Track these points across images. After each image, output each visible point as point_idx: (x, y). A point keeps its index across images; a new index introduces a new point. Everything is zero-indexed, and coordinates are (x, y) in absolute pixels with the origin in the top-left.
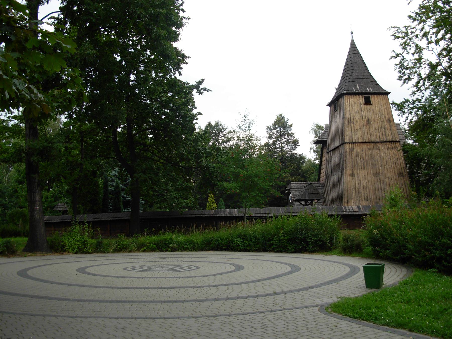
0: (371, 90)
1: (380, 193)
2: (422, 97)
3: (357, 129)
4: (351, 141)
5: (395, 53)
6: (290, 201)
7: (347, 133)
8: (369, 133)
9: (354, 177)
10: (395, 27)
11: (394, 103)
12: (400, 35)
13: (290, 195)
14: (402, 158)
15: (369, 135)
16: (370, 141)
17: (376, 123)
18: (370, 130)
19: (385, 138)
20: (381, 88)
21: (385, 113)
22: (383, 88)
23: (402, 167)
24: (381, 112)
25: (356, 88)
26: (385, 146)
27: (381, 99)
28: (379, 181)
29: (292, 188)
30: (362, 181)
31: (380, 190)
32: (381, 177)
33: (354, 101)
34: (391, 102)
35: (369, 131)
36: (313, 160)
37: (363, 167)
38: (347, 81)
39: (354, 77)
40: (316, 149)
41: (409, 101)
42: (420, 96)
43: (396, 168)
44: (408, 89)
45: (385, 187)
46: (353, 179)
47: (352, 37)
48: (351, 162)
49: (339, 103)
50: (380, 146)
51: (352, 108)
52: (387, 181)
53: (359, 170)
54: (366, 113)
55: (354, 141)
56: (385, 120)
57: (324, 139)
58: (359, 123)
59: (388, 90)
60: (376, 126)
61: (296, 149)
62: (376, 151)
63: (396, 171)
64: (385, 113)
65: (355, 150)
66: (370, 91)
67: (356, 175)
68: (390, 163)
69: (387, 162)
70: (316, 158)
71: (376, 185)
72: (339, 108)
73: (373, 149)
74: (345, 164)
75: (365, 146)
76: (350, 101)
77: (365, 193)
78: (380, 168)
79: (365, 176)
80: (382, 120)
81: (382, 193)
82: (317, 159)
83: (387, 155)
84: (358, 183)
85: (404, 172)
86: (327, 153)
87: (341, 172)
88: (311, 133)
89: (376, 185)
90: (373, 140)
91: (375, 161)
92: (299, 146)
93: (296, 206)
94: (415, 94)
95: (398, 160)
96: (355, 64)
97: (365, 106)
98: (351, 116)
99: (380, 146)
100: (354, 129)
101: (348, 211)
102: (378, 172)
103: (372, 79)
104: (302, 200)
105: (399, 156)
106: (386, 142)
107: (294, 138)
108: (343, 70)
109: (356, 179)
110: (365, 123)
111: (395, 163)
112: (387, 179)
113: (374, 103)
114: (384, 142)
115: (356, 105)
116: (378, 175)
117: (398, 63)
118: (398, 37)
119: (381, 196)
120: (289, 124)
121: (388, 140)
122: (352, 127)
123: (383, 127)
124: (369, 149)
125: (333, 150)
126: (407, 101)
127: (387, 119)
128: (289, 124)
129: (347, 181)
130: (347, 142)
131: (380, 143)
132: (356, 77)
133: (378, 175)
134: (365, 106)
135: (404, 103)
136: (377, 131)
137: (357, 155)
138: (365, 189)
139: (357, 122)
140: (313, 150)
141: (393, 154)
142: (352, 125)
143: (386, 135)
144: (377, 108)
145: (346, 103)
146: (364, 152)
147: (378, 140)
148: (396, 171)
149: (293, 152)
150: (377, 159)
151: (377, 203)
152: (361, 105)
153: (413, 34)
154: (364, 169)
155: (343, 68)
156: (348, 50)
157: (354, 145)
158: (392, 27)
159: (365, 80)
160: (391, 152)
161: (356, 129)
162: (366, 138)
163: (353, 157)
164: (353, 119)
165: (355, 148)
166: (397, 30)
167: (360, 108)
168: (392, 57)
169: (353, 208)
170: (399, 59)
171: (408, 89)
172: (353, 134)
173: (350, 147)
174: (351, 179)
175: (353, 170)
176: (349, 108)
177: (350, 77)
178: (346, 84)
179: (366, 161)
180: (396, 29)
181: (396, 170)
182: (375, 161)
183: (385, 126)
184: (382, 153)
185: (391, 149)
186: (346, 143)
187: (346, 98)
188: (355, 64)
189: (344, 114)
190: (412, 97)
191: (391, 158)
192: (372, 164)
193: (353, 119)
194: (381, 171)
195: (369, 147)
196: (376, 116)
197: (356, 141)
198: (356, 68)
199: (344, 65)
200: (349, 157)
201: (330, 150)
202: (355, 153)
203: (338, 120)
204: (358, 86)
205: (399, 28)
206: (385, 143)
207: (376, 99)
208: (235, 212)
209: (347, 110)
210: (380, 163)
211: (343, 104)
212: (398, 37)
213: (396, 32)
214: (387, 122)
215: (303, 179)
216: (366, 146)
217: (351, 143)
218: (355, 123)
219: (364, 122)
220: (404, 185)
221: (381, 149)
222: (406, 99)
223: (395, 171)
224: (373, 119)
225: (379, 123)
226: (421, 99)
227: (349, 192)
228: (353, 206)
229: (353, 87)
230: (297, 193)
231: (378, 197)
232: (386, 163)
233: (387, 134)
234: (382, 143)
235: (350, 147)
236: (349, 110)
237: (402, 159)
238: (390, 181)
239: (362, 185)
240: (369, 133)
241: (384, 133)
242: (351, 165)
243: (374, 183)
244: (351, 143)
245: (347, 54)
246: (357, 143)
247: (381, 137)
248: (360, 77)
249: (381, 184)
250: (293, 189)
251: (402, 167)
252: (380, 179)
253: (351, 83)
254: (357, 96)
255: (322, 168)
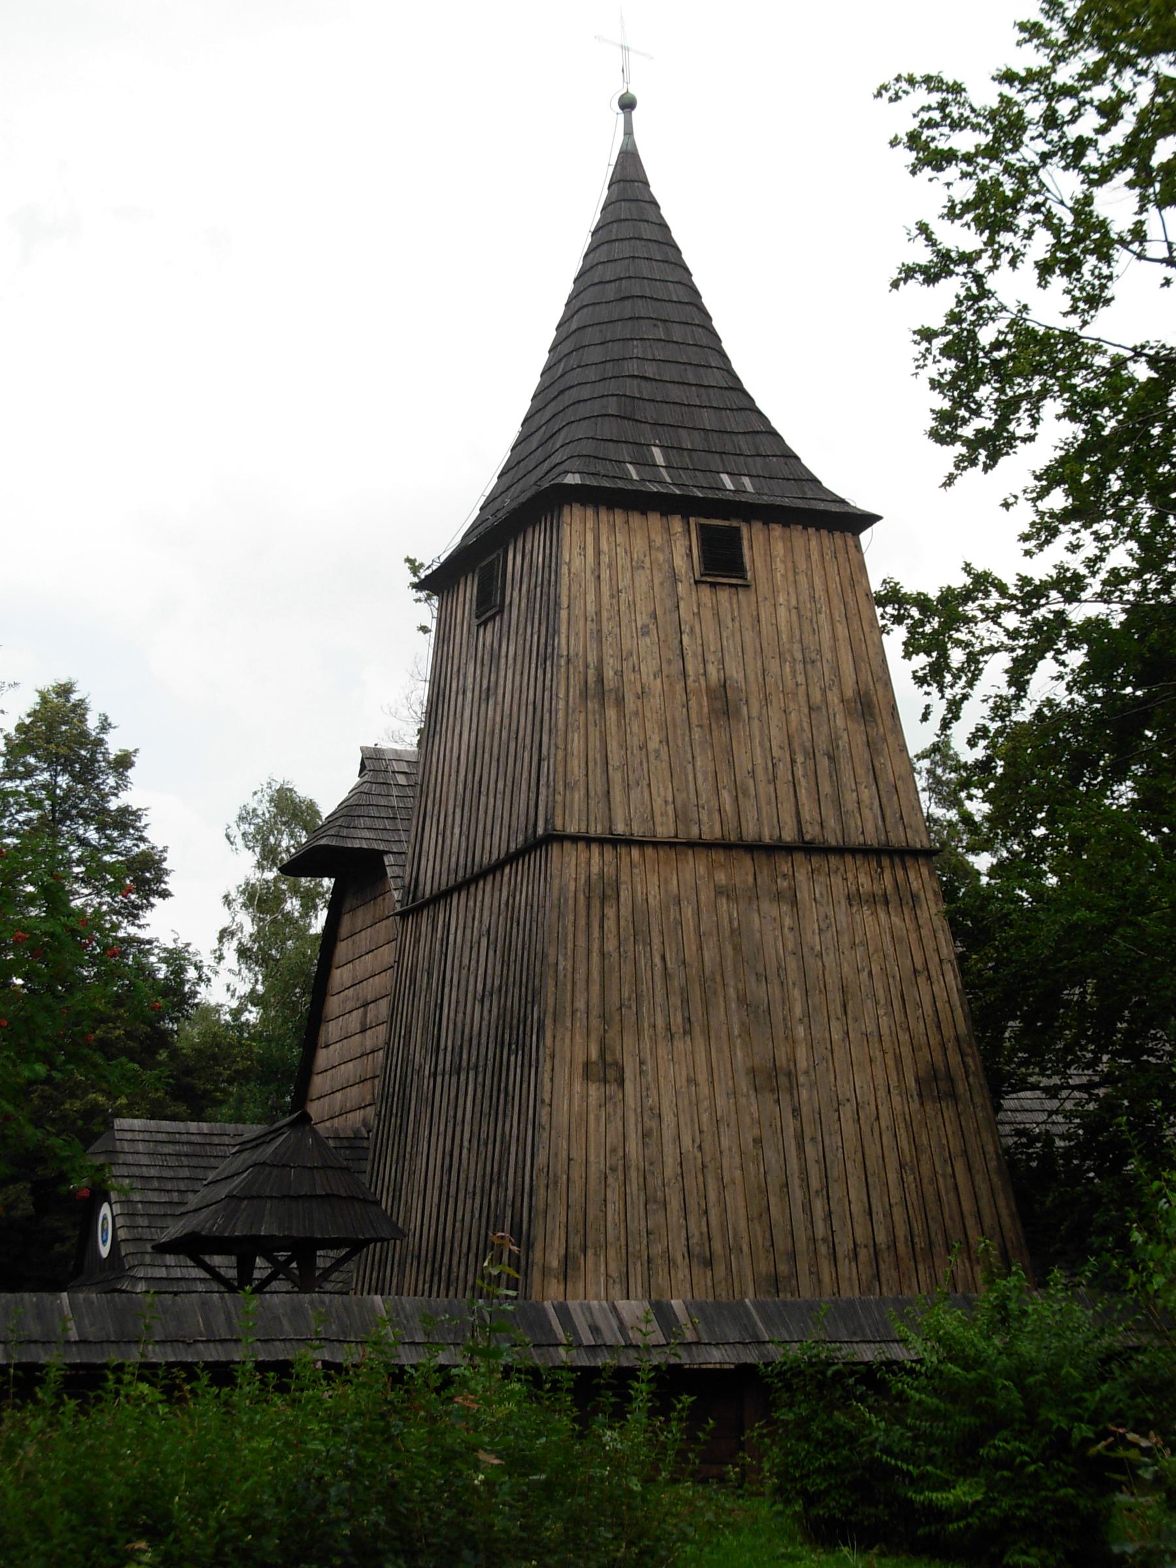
0: (750, 488)
1: (798, 1214)
2: (1092, 563)
3: (643, 747)
4: (597, 830)
5: (934, 244)
6: (105, 1251)
7: (576, 767)
8: (725, 779)
9: (613, 1088)
10: (932, 82)
11: (893, 596)
12: (965, 141)
13: (105, 1210)
14: (947, 967)
15: (726, 796)
16: (733, 838)
17: (775, 715)
18: (731, 764)
19: (831, 822)
20: (815, 481)
21: (835, 649)
22: (826, 484)
23: (948, 1032)
24: (809, 639)
25: (645, 463)
26: (837, 880)
27: (815, 556)
28: (790, 1125)
29: (122, 1158)
30: (668, 1118)
31: (797, 1193)
32: (804, 1094)
33: (629, 552)
34: (876, 586)
35: (723, 767)
36: (234, 1004)
37: (678, 1019)
38: (584, 410)
39: (632, 388)
40: (254, 938)
41: (1002, 589)
42: (1083, 554)
43: (904, 1037)
44: (1006, 505)
45: (835, 1172)
46: (606, 1101)
47: (629, 132)
48: (595, 974)
49: (514, 562)
50: (801, 876)
51: (616, 593)
52: (849, 1127)
53: (654, 1040)
54: (711, 637)
55: (620, 828)
56: (834, 698)
57: (357, 844)
58: (656, 701)
59: (861, 502)
60: (774, 731)
61: (147, 917)
62: (768, 908)
63: (908, 1062)
64: (835, 649)
65: (624, 894)
66: (740, 490)
67: (628, 1074)
68: (869, 1003)
69: (844, 990)
70: (253, 991)
71: (771, 1155)
72: (515, 597)
73: (754, 895)
74: (551, 982)
75: (694, 867)
76: (604, 546)
77: (692, 1202)
78: (801, 1031)
79: (692, 1081)
80: (817, 696)
81: (808, 1209)
82: (253, 998)
83: (845, 939)
84: (646, 1135)
85: (958, 1072)
86: (403, 915)
87: (520, 1045)
88: (239, 841)
89: (771, 1155)
90: (750, 832)
91: (765, 978)
92: (165, 894)
93: (141, 1287)
94: (1054, 533)
95: (922, 980)
96: (642, 308)
97: (705, 592)
98: (608, 651)
99: (801, 876)
100: (624, 746)
101: (587, 1338)
102: (782, 1061)
103: (753, 416)
104: (221, 1245)
105: (930, 953)
106: (841, 851)
107: (142, 839)
108: (552, 350)
109: (630, 1101)
110: (700, 706)
111: (897, 1004)
112: (847, 1111)
113: (762, 574)
114: (826, 850)
115: (642, 578)
116: (783, 1080)
117: (938, 323)
118: (939, 159)
119: (801, 1235)
120: (114, 745)
121: (856, 839)
122: (613, 729)
123: (822, 745)
124: (719, 891)
125: (458, 888)
126: (982, 582)
127: (849, 693)
128: (114, 745)
129: (561, 1118)
130: (572, 829)
131: (799, 857)
132: (647, 390)
133: (783, 1080)
134: (705, 592)
135: (967, 595)
136: (783, 770)
137: (640, 933)
138: (690, 1183)
139: (642, 695)
140: (234, 944)
141: (887, 938)
142: (611, 713)
143: (838, 802)
144: (782, 612)
145: (577, 563)
146: (688, 912)
147: (789, 835)
148: (908, 1062)
149: (127, 930)
150: (781, 969)
151: (775, 1282)
152: (675, 579)
153: (1054, 135)
154: (688, 1032)
155: (549, 335)
156: (591, 216)
157: (618, 857)
158: (911, 81)
159: (707, 419)
160: (872, 923)
161: (635, 742)
162: (704, 817)
163: (611, 945)
164: (620, 674)
165: (624, 877)
166: (943, 106)
167: (669, 604)
168: (909, 272)
169: (625, 1315)
170: (951, 288)
171: (1006, 505)
172: (616, 777)
173: (595, 869)
174: (593, 1101)
175: (612, 1034)
176: (591, 597)
177: (600, 389)
178: (580, 431)
179: (703, 979)
180: (935, 98)
181: (906, 1050)
182: (765, 978)
183: (833, 740)
184: (811, 926)
185: (872, 900)
186: (562, 838)
187: (577, 526)
188: (642, 308)
189: (556, 632)
190: (1028, 553)
191: (876, 969)
192: (742, 1000)
193: (620, 674)
194: (802, 1053)
195: (721, 877)
196: (774, 666)
197: (637, 830)
198: (645, 329)
199: (557, 312)
200: (582, 941)
201: (427, 889)
202: (625, 911)
203: (508, 679)
204: (657, 452)
205: (957, 89)
206: (834, 860)
207: (779, 548)
208: (734, 1006)
209: (577, 611)
210: (796, 993)
211: (553, 564)
212: (948, 157)
213: (936, 115)
214: (848, 713)
215: (182, 1108)
216: (702, 870)
217: (601, 841)
218: (631, 704)
219: (693, 703)
220: (959, 1166)
221: (804, 895)
222: (979, 568)
223: (898, 1059)
224: (754, 688)
225: (793, 716)
226: (1083, 571)
227: (576, 1194)
228: (621, 1304)
229: (625, 452)
230: (154, 1197)
231: (782, 1243)
232: (836, 997)
233: (850, 798)
234: (816, 860)
235: (595, 869)
236: (591, 608)
237: (950, 977)
238: (866, 1129)
239: (670, 1150)
240: (725, 779)
241: (826, 788)
242: (595, 1000)
243: (758, 1141)
244: (601, 841)
245: (583, 242)
246: (642, 844)
247: (806, 815)
248: (676, 393)
249: (801, 1147)
250: (125, 1171)
251: (948, 1032)
252: (796, 1112)
253: (608, 429)
254: (655, 519)
255: (322, 1040)
